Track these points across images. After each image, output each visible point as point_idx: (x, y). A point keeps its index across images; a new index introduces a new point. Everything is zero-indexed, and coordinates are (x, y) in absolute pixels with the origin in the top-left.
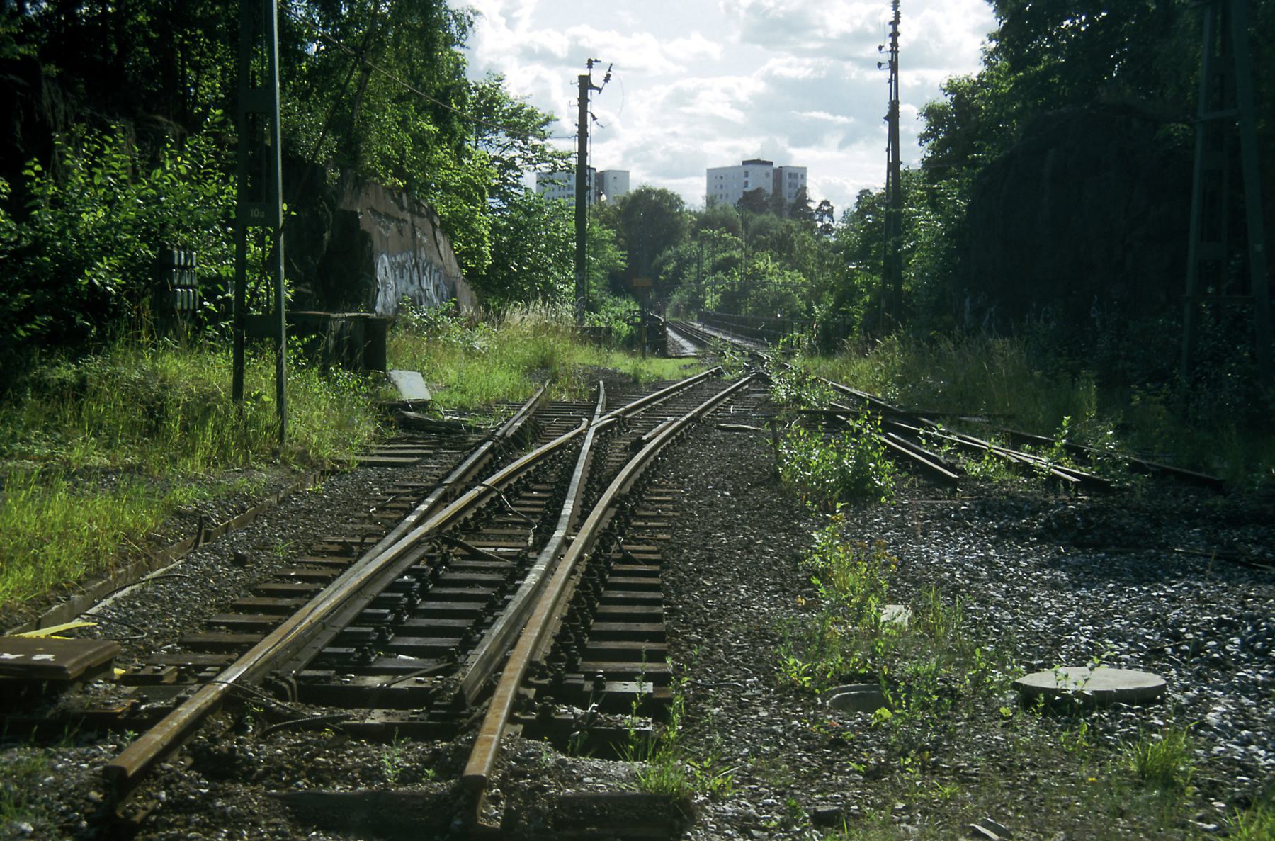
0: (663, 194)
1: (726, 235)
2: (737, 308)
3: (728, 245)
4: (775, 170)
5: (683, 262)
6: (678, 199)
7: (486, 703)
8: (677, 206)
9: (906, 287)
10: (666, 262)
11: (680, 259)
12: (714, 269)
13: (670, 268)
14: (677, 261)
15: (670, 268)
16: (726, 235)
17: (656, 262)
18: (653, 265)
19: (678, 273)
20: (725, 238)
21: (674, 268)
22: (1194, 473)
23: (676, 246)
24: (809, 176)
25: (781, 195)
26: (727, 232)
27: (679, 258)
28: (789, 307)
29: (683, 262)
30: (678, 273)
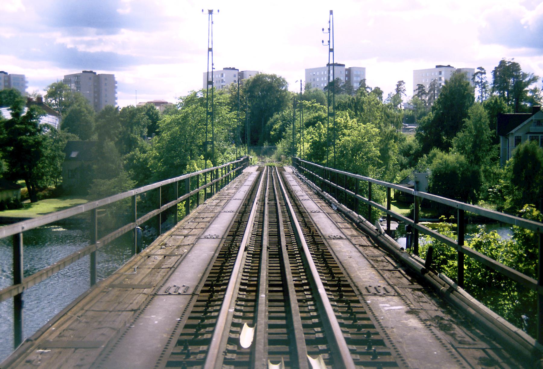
0: (273, 77)
1: (316, 104)
2: (324, 154)
3: (317, 110)
4: (346, 70)
5: (286, 122)
6: (284, 81)
7: (256, 324)
8: (283, 86)
9: (524, 81)
10: (275, 122)
11: (285, 120)
12: (308, 125)
13: (277, 126)
14: (282, 121)
15: (277, 126)
16: (316, 104)
17: (269, 123)
18: (267, 125)
19: (283, 129)
20: (316, 107)
21: (281, 126)
22: (96, 233)
23: (282, 111)
24: (367, 71)
25: (350, 84)
26: (317, 102)
27: (284, 119)
28: (366, 153)
29: (286, 122)
30: (283, 129)
